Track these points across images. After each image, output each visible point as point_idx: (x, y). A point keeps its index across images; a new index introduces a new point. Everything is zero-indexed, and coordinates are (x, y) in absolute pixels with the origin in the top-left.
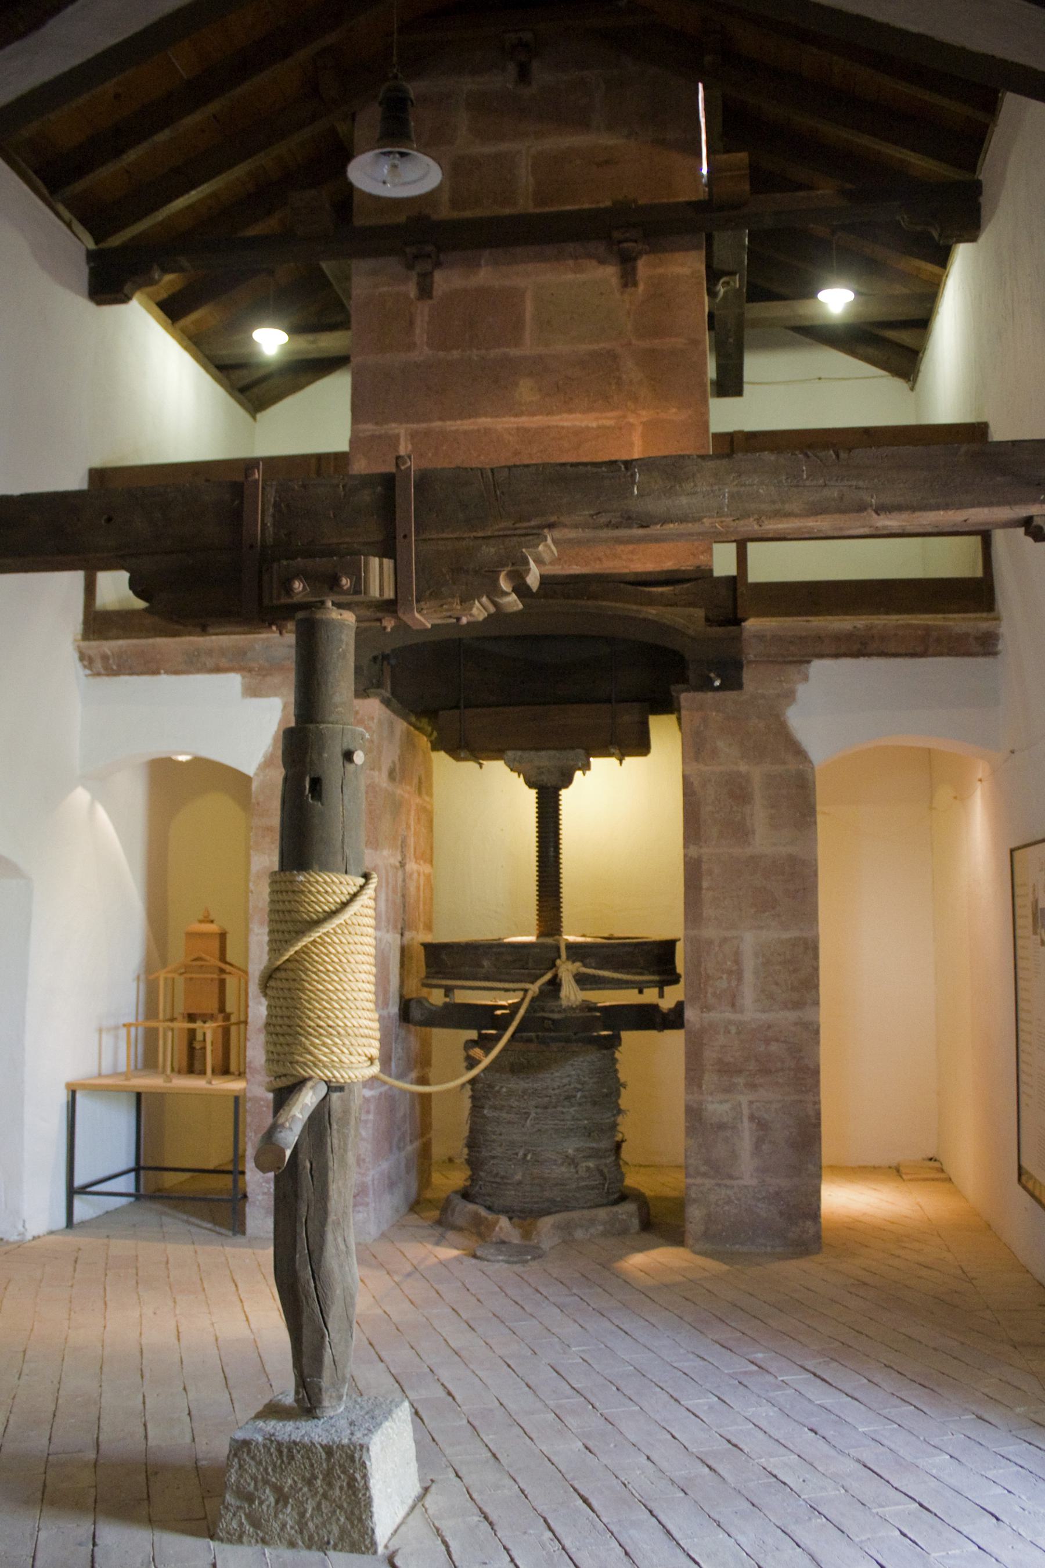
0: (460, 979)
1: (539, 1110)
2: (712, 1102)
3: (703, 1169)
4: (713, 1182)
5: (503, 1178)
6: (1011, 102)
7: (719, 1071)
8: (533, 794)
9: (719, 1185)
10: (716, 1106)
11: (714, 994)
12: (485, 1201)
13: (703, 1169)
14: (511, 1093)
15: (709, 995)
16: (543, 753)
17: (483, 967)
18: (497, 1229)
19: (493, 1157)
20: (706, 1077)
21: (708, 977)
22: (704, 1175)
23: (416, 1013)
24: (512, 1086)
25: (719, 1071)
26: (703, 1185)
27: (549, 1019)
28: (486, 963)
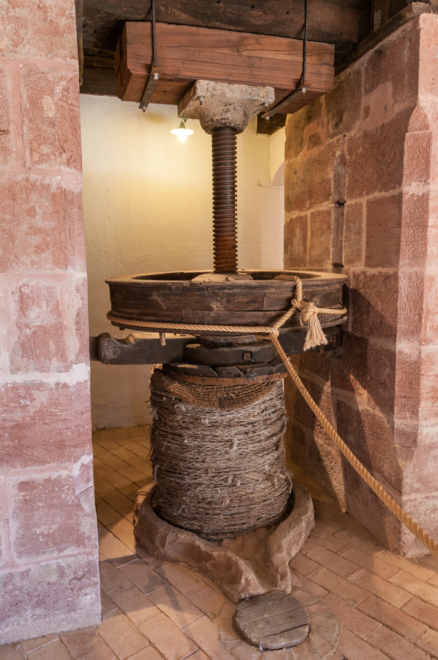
0: (180, 323)
1: (240, 437)
2: (427, 427)
3: (417, 485)
4: (424, 496)
5: (209, 503)
6: (127, 23)
7: (432, 398)
8: (209, 138)
9: (427, 497)
10: (429, 429)
11: (432, 328)
12: (192, 525)
13: (417, 485)
14: (214, 425)
15: (428, 329)
16: (235, 86)
17: (211, 309)
18: (243, 581)
19: (200, 484)
20: (423, 404)
21: (429, 311)
22: (417, 491)
23: (108, 351)
24: (217, 417)
25: (432, 398)
26: (416, 499)
27: (247, 352)
28: (214, 306)
